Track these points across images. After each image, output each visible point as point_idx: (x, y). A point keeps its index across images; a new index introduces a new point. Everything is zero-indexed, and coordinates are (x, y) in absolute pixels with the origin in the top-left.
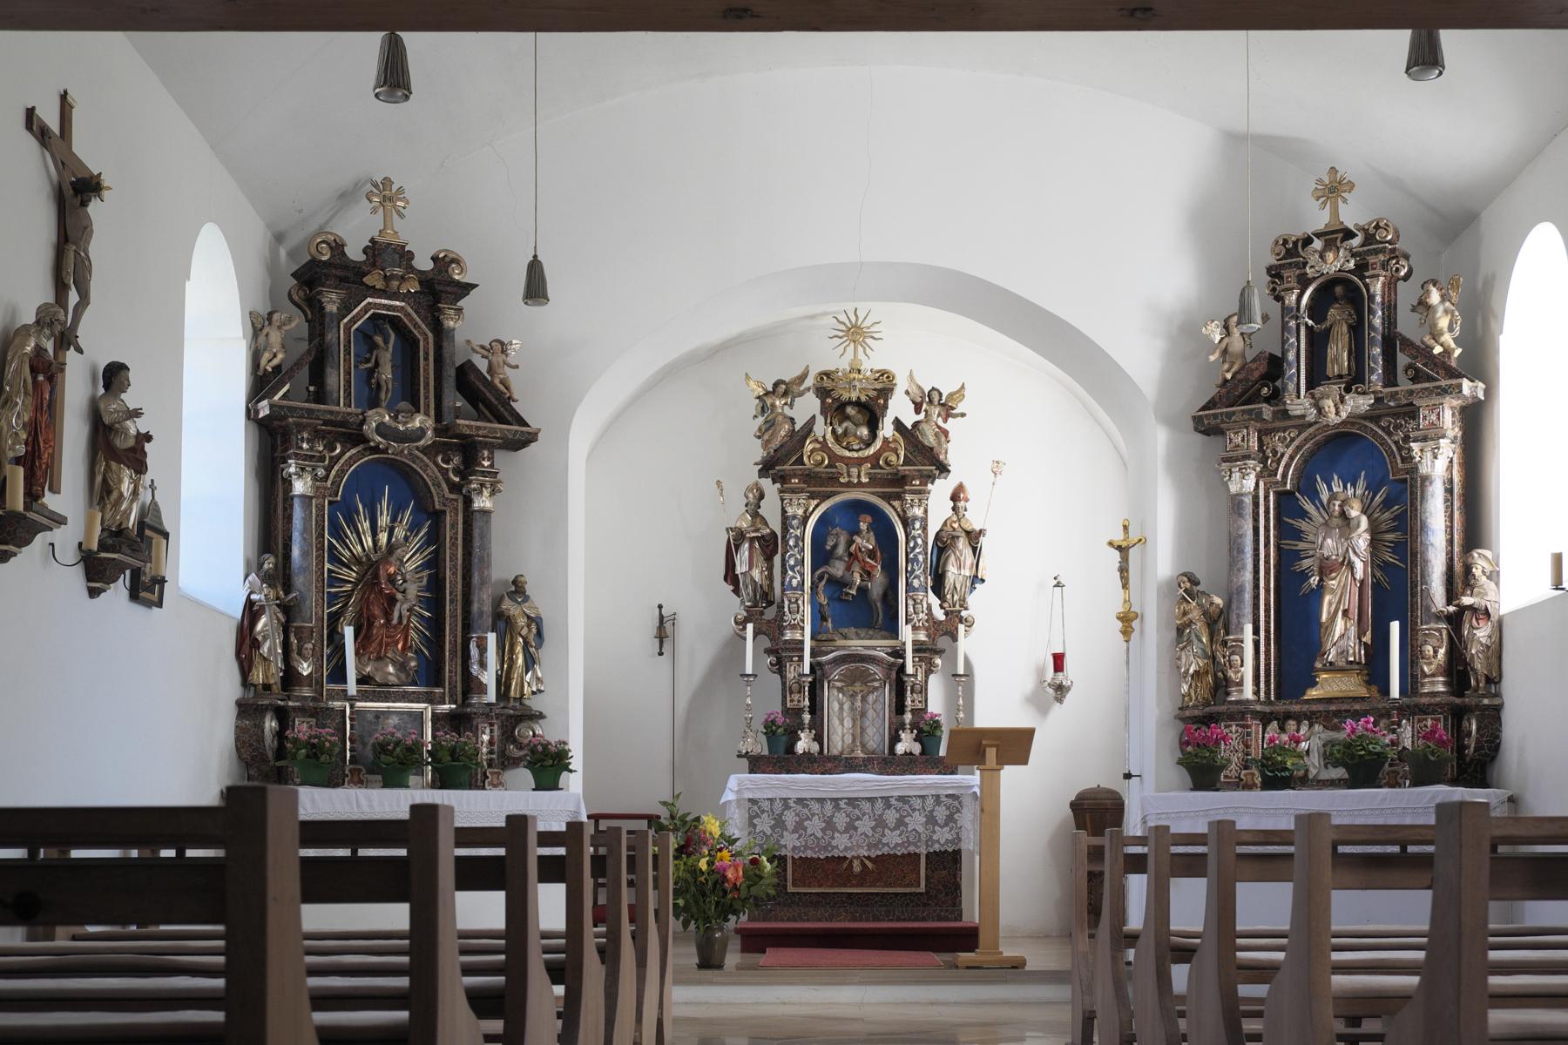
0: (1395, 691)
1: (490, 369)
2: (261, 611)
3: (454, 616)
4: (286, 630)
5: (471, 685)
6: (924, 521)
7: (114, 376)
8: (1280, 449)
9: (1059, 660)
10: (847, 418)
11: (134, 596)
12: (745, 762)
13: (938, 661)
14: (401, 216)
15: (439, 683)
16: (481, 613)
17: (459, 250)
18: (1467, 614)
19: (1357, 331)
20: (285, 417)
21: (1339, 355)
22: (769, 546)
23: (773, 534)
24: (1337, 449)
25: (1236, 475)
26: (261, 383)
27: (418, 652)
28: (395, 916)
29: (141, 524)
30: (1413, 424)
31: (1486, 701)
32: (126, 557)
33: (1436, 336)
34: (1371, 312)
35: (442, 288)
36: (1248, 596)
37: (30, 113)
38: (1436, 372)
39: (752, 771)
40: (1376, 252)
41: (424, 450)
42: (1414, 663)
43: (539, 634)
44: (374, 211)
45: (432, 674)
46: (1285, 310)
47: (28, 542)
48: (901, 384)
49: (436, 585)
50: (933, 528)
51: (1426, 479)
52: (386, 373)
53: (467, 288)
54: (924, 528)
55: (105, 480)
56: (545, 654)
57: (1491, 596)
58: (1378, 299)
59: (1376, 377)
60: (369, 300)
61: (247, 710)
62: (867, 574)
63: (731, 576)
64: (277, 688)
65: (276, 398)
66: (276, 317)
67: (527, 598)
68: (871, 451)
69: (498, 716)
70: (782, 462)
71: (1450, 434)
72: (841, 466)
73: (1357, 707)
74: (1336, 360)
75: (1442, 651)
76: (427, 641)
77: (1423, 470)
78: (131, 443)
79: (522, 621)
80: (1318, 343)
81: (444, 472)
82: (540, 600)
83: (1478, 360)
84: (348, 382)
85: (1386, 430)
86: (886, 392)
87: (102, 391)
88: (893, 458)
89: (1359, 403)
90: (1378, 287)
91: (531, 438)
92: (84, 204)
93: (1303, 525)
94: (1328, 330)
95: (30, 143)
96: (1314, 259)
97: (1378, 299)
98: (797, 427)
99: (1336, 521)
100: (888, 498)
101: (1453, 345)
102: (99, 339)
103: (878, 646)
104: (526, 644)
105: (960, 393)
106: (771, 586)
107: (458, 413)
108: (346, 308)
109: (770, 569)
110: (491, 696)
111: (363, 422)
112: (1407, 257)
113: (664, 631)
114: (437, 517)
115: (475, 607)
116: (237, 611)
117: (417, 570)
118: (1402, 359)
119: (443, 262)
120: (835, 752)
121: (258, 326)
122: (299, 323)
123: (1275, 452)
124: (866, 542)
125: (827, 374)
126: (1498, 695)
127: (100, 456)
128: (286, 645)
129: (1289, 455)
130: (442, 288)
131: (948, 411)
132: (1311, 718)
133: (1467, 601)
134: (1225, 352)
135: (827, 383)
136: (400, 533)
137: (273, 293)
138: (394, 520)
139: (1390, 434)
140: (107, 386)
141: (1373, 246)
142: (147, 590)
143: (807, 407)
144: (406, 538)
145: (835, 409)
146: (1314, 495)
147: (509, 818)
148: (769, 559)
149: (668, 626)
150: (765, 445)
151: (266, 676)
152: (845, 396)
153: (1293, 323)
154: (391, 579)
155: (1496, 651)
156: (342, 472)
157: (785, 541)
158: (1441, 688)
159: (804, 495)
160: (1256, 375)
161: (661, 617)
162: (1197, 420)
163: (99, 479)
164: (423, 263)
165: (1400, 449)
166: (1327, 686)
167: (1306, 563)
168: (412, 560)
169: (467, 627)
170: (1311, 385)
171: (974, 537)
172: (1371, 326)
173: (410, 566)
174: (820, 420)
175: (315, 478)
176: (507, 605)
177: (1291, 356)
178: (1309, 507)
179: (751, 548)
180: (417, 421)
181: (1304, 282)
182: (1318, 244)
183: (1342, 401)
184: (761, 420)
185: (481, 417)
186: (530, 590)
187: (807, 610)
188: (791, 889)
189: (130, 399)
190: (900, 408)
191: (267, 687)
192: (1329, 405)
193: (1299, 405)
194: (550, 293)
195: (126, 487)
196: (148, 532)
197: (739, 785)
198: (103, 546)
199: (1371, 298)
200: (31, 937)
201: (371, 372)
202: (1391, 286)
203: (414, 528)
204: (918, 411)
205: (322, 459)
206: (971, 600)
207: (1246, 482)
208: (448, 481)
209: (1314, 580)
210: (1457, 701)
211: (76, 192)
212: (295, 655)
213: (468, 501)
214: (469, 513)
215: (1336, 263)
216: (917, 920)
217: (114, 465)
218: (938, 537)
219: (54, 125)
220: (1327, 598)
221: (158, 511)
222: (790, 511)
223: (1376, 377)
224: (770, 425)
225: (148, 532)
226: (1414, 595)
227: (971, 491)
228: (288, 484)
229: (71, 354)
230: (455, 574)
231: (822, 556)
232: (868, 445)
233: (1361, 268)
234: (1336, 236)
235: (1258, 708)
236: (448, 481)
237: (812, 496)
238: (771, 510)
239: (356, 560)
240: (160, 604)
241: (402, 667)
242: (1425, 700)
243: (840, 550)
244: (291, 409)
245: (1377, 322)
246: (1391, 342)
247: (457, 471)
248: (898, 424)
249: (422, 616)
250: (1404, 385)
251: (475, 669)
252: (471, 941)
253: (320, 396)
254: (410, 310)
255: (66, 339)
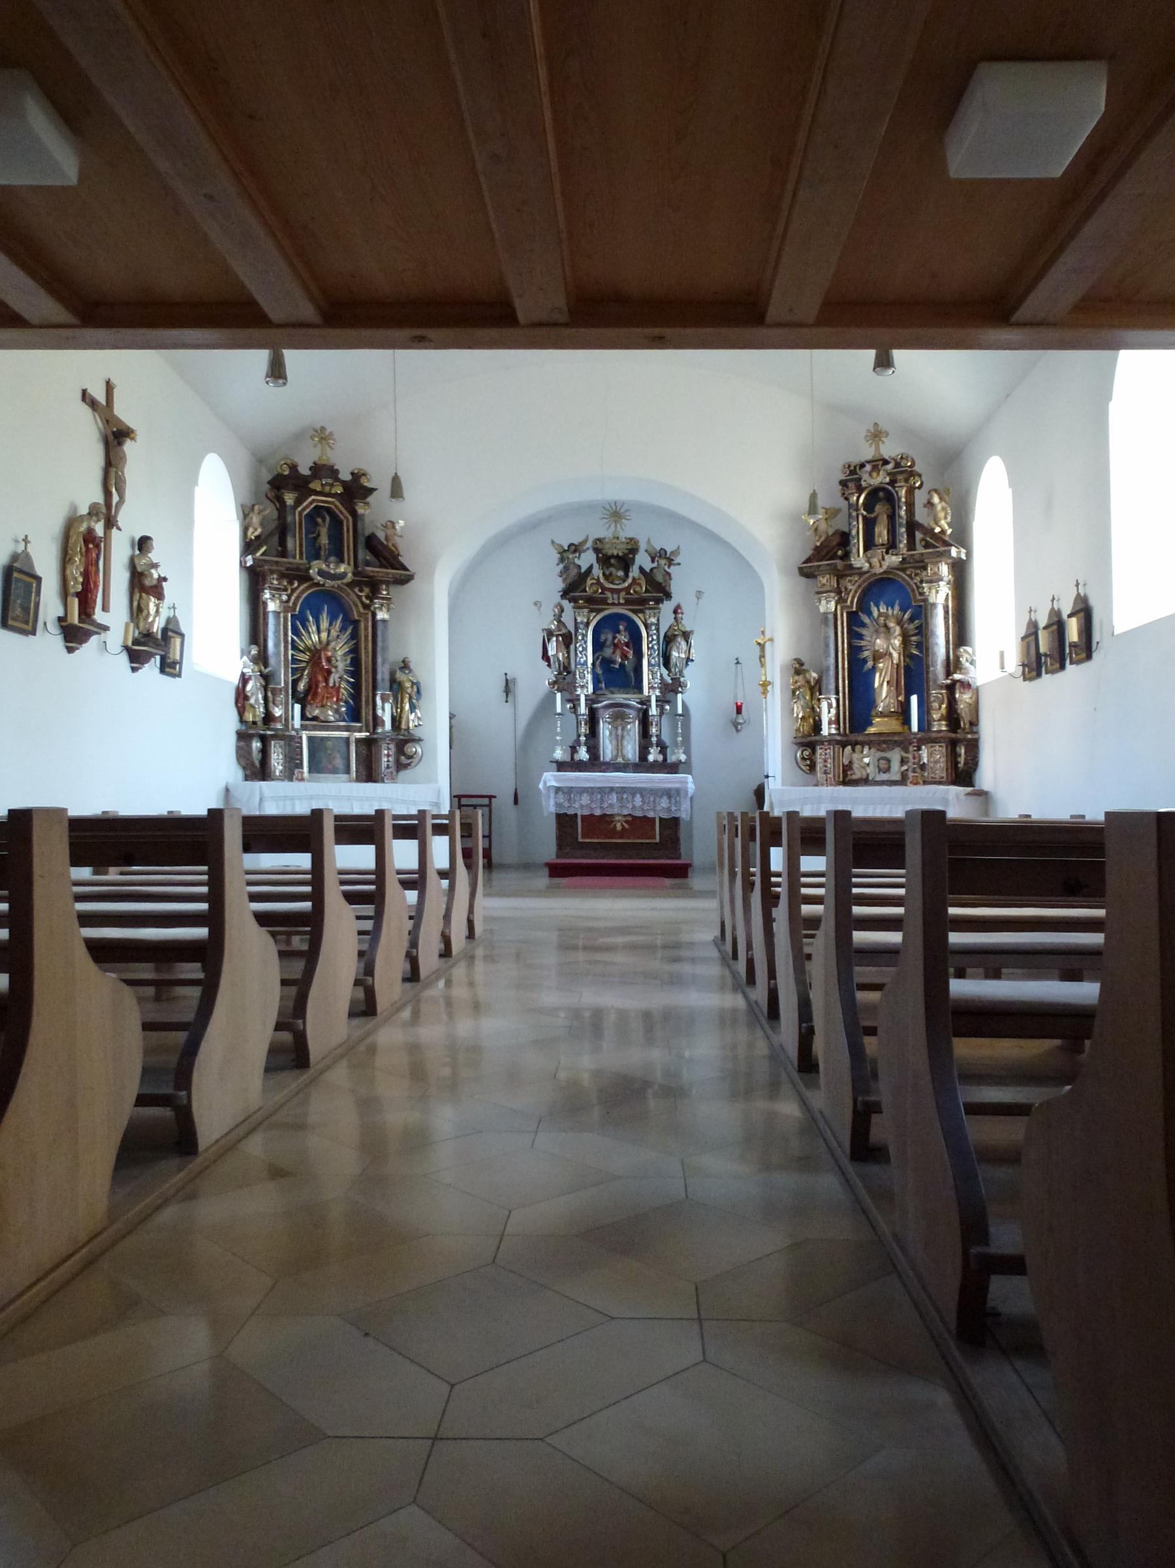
0: (915, 727)
1: (387, 539)
2: (250, 678)
3: (367, 681)
4: (265, 688)
5: (377, 721)
6: (657, 625)
7: (143, 544)
8: (850, 587)
9: (739, 709)
10: (612, 565)
11: (162, 671)
12: (554, 765)
13: (668, 707)
14: (331, 448)
15: (358, 720)
16: (383, 680)
17: (364, 467)
18: (958, 685)
19: (892, 517)
20: (262, 566)
21: (882, 534)
22: (567, 640)
23: (570, 632)
24: (879, 586)
25: (823, 602)
26: (248, 547)
27: (346, 702)
28: (303, 860)
29: (165, 630)
30: (924, 573)
31: (969, 736)
32: (154, 647)
33: (937, 523)
34: (900, 508)
35: (356, 490)
36: (832, 672)
37: (84, 392)
38: (937, 543)
39: (559, 770)
40: (902, 472)
41: (348, 585)
42: (929, 713)
43: (418, 692)
44: (315, 446)
45: (355, 714)
46: (850, 506)
47: (85, 641)
48: (643, 546)
49: (356, 663)
50: (663, 630)
51: (934, 605)
52: (324, 540)
53: (371, 491)
54: (658, 630)
55: (139, 605)
56: (423, 703)
57: (971, 674)
58: (903, 500)
59: (903, 544)
60: (313, 497)
61: (243, 737)
62: (624, 656)
63: (545, 656)
64: (260, 724)
65: (258, 554)
66: (256, 507)
67: (410, 671)
68: (626, 584)
69: (392, 740)
70: (575, 588)
71: (946, 579)
72: (609, 594)
73: (896, 738)
74: (880, 535)
75: (944, 706)
76: (352, 696)
77: (931, 600)
78: (155, 582)
79: (408, 685)
80: (870, 525)
81: (359, 597)
82: (419, 672)
83: (962, 536)
84: (301, 545)
85: (910, 576)
86: (634, 551)
87: (137, 552)
88: (638, 589)
89: (894, 560)
90: (903, 492)
91: (410, 578)
92: (120, 444)
93: (864, 632)
94: (876, 518)
95: (86, 410)
96: (865, 477)
97: (903, 500)
98: (583, 570)
99: (883, 629)
100: (635, 612)
101: (946, 527)
102: (133, 519)
103: (633, 700)
104: (410, 698)
105: (676, 552)
106: (569, 663)
107: (368, 564)
108: (298, 502)
109: (568, 653)
110: (388, 726)
111: (310, 568)
112: (920, 476)
113: (508, 688)
114: (356, 623)
115: (379, 677)
116: (235, 680)
117: (345, 655)
118: (919, 535)
119: (357, 476)
120: (607, 759)
121: (246, 513)
122: (271, 510)
123: (846, 589)
124: (623, 638)
125: (599, 540)
126: (977, 733)
127: (136, 590)
128: (266, 698)
129: (852, 586)
130: (356, 490)
131: (670, 562)
132: (870, 744)
133: (957, 676)
134: (816, 530)
135: (599, 545)
136: (334, 633)
137: (256, 493)
138: (331, 624)
139: (912, 579)
140: (140, 549)
141: (903, 471)
142: (169, 667)
143: (587, 559)
144: (338, 637)
145: (605, 560)
146: (870, 614)
147: (313, 811)
148: (567, 647)
149: (511, 685)
150: (564, 580)
151: (254, 716)
152: (610, 553)
153: (854, 514)
154: (329, 660)
155: (975, 708)
156: (298, 598)
157: (576, 638)
158: (944, 728)
159: (586, 610)
160: (835, 543)
161: (507, 680)
162: (801, 570)
163: (135, 604)
164: (345, 476)
165: (918, 588)
166: (878, 726)
167: (866, 654)
168: (339, 651)
169: (375, 688)
170: (866, 549)
171: (686, 636)
172: (900, 517)
173: (339, 653)
174: (596, 566)
175: (282, 602)
176: (400, 676)
177: (854, 532)
178: (866, 620)
179: (557, 641)
180: (342, 568)
181: (860, 490)
182: (868, 467)
183: (883, 559)
184: (561, 566)
185: (382, 566)
186: (412, 666)
187: (589, 677)
188: (580, 840)
189: (154, 556)
190: (642, 560)
191: (254, 723)
192: (875, 561)
193: (859, 560)
194: (405, 495)
195: (152, 608)
196: (170, 634)
197: (550, 779)
198: (134, 644)
199: (899, 499)
200: (95, 873)
201: (316, 539)
202: (911, 491)
203: (343, 629)
204: (653, 561)
205: (285, 590)
206: (685, 672)
207: (829, 605)
208: (362, 602)
209: (870, 664)
210: (953, 735)
211: (116, 437)
212: (271, 704)
213: (374, 615)
214: (375, 622)
215: (880, 479)
216: (654, 858)
217: (144, 595)
218: (666, 636)
219: (102, 399)
220: (877, 675)
221: (177, 622)
222: (579, 619)
223: (903, 544)
224: (566, 568)
225: (170, 634)
226: (928, 673)
227: (685, 608)
228: (265, 604)
229: (114, 530)
230: (367, 657)
231: (598, 646)
232: (624, 581)
233: (893, 482)
234: (879, 463)
235: (838, 738)
236: (362, 602)
237: (591, 611)
238: (568, 618)
239: (308, 649)
240: (179, 676)
241: (337, 711)
242: (934, 735)
243: (608, 643)
244: (265, 561)
245: (903, 513)
246: (912, 526)
247: (367, 597)
248: (641, 569)
249: (348, 682)
250: (920, 550)
251: (379, 712)
252: (347, 876)
253: (283, 553)
254: (338, 504)
255: (110, 523)
